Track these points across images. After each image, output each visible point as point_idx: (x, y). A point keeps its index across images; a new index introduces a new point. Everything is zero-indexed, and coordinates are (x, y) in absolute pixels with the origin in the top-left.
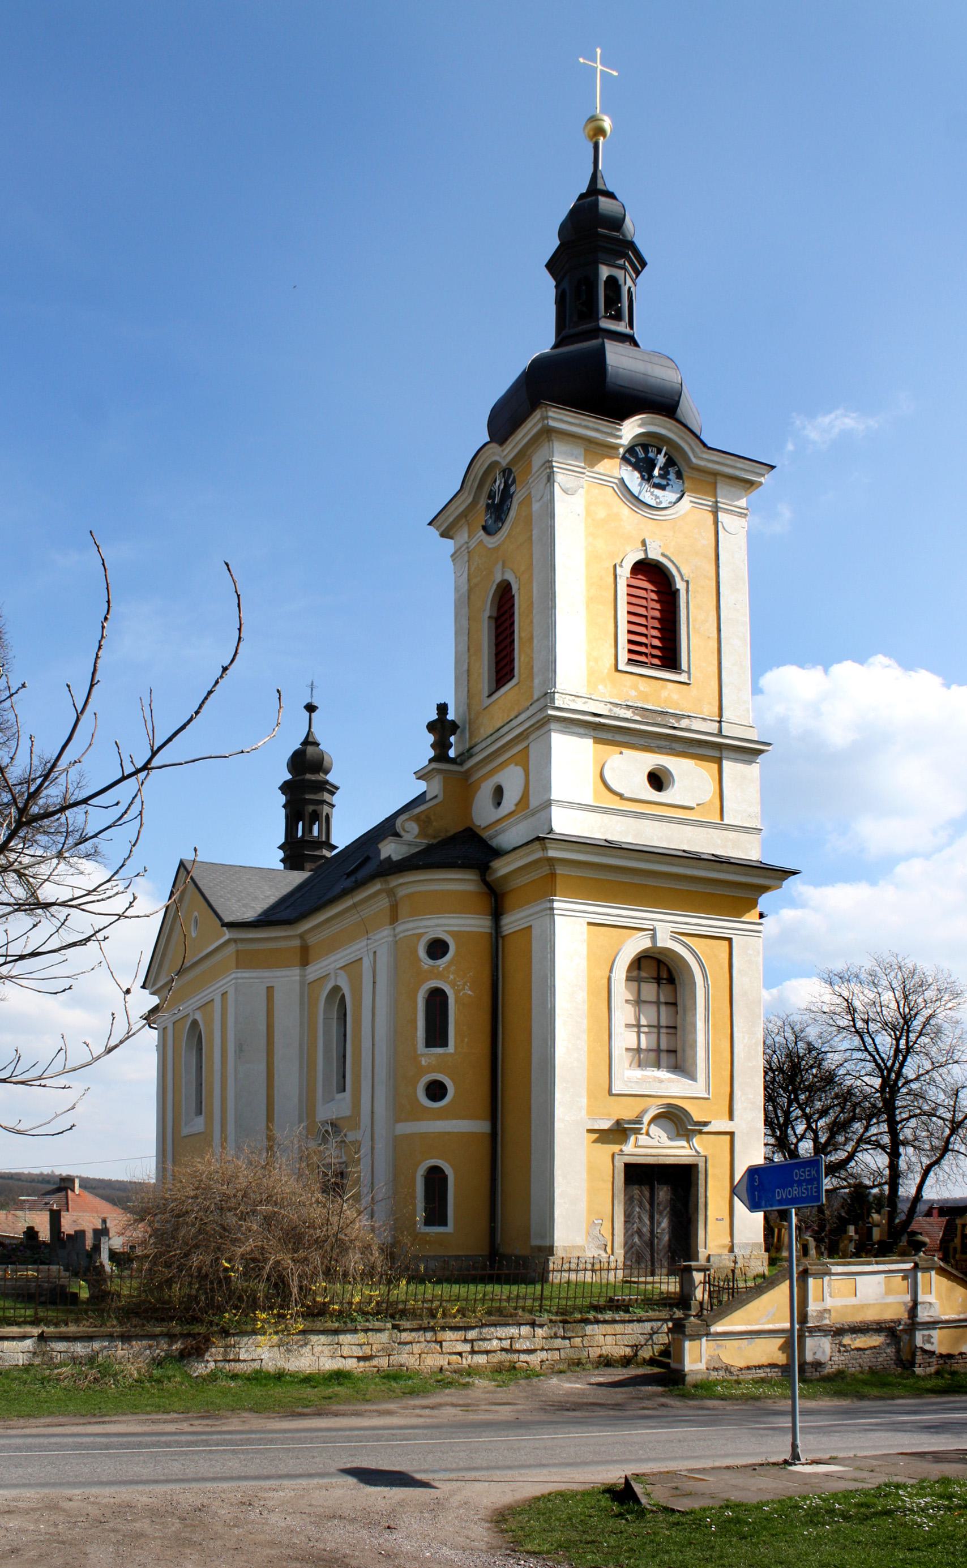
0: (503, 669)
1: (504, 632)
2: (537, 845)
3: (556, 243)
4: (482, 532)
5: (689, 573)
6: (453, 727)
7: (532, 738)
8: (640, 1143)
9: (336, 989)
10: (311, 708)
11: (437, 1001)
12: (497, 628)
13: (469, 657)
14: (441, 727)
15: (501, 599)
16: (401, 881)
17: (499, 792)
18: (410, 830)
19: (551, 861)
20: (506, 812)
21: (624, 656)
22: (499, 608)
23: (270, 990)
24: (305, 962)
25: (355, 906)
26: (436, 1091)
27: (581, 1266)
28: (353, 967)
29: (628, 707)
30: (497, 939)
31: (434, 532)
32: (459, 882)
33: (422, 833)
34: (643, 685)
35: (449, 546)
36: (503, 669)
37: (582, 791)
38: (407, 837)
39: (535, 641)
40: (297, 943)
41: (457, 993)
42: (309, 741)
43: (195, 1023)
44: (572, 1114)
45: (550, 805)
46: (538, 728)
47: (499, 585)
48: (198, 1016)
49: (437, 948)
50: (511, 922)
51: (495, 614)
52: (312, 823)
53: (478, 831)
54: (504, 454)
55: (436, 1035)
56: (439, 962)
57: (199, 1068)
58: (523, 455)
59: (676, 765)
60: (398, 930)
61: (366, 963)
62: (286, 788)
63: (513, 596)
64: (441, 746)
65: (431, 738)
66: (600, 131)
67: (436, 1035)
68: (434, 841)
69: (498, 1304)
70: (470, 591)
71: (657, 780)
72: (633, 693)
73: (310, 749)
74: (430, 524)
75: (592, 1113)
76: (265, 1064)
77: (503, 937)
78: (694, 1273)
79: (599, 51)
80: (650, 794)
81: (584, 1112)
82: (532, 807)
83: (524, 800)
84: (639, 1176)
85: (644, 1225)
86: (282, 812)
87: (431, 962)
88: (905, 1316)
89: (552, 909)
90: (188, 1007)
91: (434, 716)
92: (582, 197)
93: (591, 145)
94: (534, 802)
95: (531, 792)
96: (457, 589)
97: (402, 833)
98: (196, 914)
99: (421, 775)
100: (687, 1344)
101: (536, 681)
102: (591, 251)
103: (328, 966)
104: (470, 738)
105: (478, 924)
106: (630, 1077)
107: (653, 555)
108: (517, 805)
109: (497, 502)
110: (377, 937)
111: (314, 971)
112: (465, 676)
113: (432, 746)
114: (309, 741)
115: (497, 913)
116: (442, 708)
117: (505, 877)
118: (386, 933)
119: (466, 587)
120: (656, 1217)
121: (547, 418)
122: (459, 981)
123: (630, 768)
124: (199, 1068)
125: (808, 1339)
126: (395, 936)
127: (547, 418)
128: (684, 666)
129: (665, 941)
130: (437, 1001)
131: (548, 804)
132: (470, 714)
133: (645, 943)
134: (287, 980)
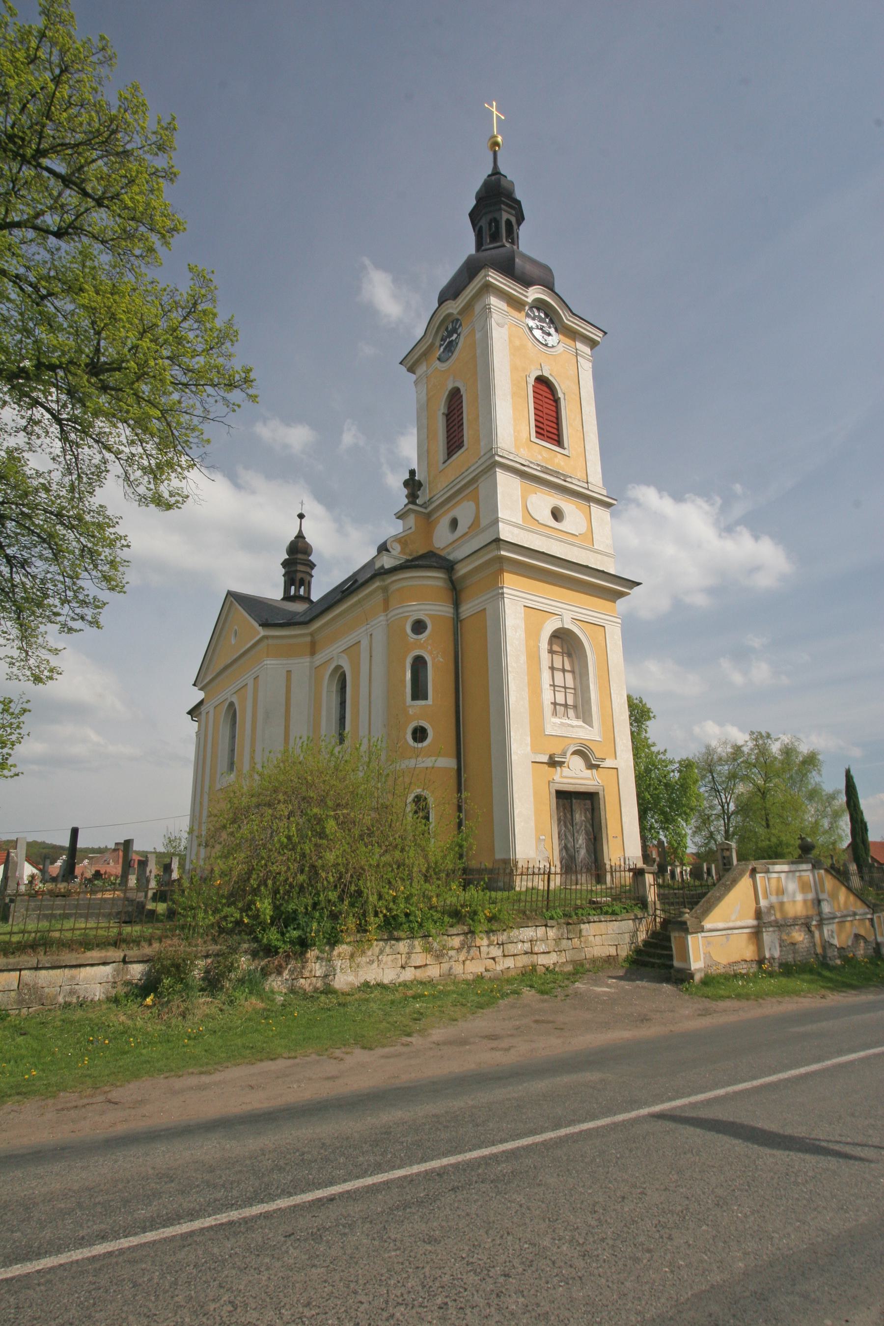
0: (454, 441)
1: (456, 422)
2: (494, 546)
3: (474, 202)
4: (438, 362)
5: (562, 388)
6: (420, 485)
7: (480, 481)
8: (564, 774)
9: (339, 667)
10: (301, 516)
11: (419, 664)
12: (447, 421)
13: (429, 443)
14: (413, 485)
15: (450, 401)
16: (394, 578)
17: (454, 523)
18: (396, 549)
19: (502, 559)
20: (460, 535)
21: (533, 434)
22: (449, 408)
23: (289, 672)
24: (313, 653)
25: (359, 601)
26: (420, 734)
27: (530, 871)
28: (353, 650)
29: (538, 465)
30: (457, 621)
31: (403, 369)
32: (434, 579)
33: (403, 551)
34: (545, 454)
35: (413, 377)
36: (454, 441)
37: (518, 512)
38: (394, 553)
39: (481, 418)
40: (308, 639)
41: (433, 659)
42: (300, 536)
43: (232, 704)
44: (521, 752)
45: (498, 522)
46: (486, 473)
47: (453, 389)
48: (235, 699)
49: (419, 627)
50: (467, 609)
51: (446, 412)
52: (300, 587)
53: (437, 552)
54: (453, 307)
55: (419, 692)
56: (421, 636)
57: (233, 737)
58: (468, 308)
59: (568, 506)
60: (389, 616)
61: (365, 644)
62: (285, 564)
63: (462, 396)
64: (412, 497)
65: (405, 492)
66: (496, 144)
67: (419, 692)
68: (410, 558)
69: (94, 933)
70: (428, 400)
71: (557, 514)
72: (540, 457)
73: (301, 540)
74: (401, 363)
75: (535, 750)
76: (283, 727)
77: (461, 621)
78: (646, 875)
79: (494, 103)
80: (552, 522)
81: (529, 748)
82: (481, 526)
83: (475, 523)
84: (566, 799)
85: (569, 841)
86: (283, 579)
87: (415, 637)
88: (812, 912)
89: (503, 593)
90: (227, 693)
91: (407, 476)
92: (489, 176)
93: (491, 154)
94: (484, 522)
95: (481, 516)
96: (418, 401)
97: (391, 550)
98: (236, 627)
99: (401, 516)
100: (689, 937)
101: (482, 444)
102: (495, 210)
103: (333, 653)
104: (430, 492)
105: (445, 610)
106: (554, 725)
107: (546, 374)
108: (469, 528)
109: (451, 332)
110: (372, 623)
111: (320, 658)
112: (424, 452)
113: (406, 496)
114: (300, 536)
115: (457, 604)
116: (412, 473)
117: (465, 577)
118: (381, 618)
119: (425, 399)
120: (576, 834)
121: (489, 275)
122: (433, 650)
123: (542, 502)
124: (233, 737)
125: (764, 934)
126: (387, 621)
127: (489, 275)
128: (566, 445)
129: (569, 625)
130: (419, 664)
131: (496, 521)
132: (429, 476)
133: (559, 625)
134: (301, 665)
